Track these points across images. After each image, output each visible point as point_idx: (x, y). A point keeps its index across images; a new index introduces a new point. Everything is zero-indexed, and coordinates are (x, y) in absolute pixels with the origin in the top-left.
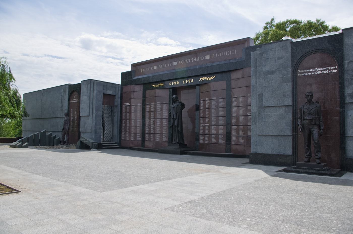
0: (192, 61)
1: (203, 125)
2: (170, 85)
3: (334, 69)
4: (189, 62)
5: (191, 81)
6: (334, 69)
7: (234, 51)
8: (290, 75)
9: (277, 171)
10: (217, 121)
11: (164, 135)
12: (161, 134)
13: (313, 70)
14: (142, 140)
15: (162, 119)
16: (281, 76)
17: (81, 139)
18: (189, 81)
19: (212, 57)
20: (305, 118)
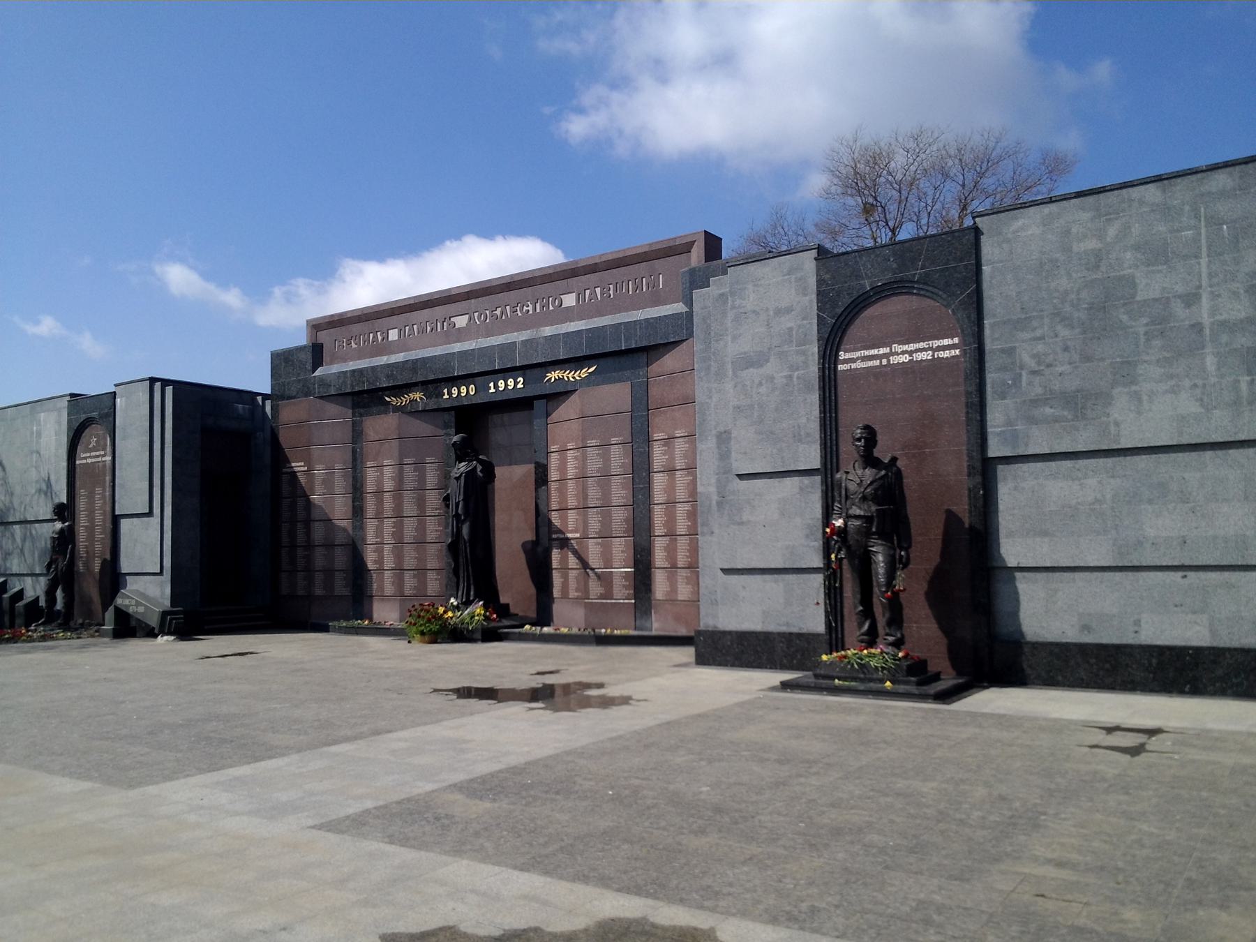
2: (492, 390)
3: (948, 348)
5: (516, 383)
9: (313, 827)
10: (606, 521)
11: (431, 575)
13: (887, 350)
15: (422, 516)
17: (119, 601)
18: (511, 383)
20: (851, 512)
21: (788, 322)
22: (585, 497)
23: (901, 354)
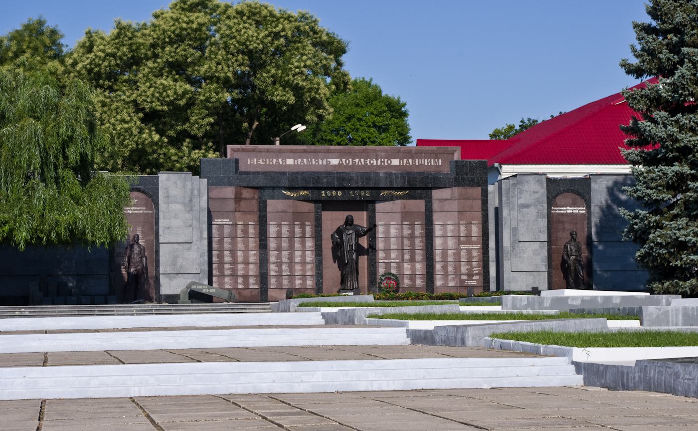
0: (369, 164)
1: (385, 261)
2: (323, 195)
3: (582, 210)
4: (361, 163)
6: (583, 210)
7: (438, 161)
8: (545, 211)
11: (308, 278)
12: (303, 277)
14: (261, 288)
16: (536, 211)
19: (403, 163)
21: (537, 196)
22: (403, 246)
23: (569, 210)
